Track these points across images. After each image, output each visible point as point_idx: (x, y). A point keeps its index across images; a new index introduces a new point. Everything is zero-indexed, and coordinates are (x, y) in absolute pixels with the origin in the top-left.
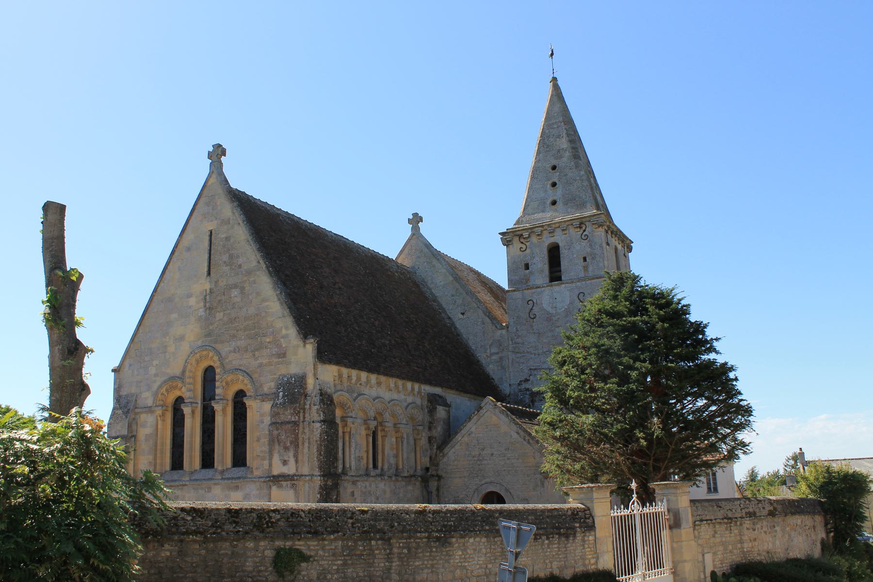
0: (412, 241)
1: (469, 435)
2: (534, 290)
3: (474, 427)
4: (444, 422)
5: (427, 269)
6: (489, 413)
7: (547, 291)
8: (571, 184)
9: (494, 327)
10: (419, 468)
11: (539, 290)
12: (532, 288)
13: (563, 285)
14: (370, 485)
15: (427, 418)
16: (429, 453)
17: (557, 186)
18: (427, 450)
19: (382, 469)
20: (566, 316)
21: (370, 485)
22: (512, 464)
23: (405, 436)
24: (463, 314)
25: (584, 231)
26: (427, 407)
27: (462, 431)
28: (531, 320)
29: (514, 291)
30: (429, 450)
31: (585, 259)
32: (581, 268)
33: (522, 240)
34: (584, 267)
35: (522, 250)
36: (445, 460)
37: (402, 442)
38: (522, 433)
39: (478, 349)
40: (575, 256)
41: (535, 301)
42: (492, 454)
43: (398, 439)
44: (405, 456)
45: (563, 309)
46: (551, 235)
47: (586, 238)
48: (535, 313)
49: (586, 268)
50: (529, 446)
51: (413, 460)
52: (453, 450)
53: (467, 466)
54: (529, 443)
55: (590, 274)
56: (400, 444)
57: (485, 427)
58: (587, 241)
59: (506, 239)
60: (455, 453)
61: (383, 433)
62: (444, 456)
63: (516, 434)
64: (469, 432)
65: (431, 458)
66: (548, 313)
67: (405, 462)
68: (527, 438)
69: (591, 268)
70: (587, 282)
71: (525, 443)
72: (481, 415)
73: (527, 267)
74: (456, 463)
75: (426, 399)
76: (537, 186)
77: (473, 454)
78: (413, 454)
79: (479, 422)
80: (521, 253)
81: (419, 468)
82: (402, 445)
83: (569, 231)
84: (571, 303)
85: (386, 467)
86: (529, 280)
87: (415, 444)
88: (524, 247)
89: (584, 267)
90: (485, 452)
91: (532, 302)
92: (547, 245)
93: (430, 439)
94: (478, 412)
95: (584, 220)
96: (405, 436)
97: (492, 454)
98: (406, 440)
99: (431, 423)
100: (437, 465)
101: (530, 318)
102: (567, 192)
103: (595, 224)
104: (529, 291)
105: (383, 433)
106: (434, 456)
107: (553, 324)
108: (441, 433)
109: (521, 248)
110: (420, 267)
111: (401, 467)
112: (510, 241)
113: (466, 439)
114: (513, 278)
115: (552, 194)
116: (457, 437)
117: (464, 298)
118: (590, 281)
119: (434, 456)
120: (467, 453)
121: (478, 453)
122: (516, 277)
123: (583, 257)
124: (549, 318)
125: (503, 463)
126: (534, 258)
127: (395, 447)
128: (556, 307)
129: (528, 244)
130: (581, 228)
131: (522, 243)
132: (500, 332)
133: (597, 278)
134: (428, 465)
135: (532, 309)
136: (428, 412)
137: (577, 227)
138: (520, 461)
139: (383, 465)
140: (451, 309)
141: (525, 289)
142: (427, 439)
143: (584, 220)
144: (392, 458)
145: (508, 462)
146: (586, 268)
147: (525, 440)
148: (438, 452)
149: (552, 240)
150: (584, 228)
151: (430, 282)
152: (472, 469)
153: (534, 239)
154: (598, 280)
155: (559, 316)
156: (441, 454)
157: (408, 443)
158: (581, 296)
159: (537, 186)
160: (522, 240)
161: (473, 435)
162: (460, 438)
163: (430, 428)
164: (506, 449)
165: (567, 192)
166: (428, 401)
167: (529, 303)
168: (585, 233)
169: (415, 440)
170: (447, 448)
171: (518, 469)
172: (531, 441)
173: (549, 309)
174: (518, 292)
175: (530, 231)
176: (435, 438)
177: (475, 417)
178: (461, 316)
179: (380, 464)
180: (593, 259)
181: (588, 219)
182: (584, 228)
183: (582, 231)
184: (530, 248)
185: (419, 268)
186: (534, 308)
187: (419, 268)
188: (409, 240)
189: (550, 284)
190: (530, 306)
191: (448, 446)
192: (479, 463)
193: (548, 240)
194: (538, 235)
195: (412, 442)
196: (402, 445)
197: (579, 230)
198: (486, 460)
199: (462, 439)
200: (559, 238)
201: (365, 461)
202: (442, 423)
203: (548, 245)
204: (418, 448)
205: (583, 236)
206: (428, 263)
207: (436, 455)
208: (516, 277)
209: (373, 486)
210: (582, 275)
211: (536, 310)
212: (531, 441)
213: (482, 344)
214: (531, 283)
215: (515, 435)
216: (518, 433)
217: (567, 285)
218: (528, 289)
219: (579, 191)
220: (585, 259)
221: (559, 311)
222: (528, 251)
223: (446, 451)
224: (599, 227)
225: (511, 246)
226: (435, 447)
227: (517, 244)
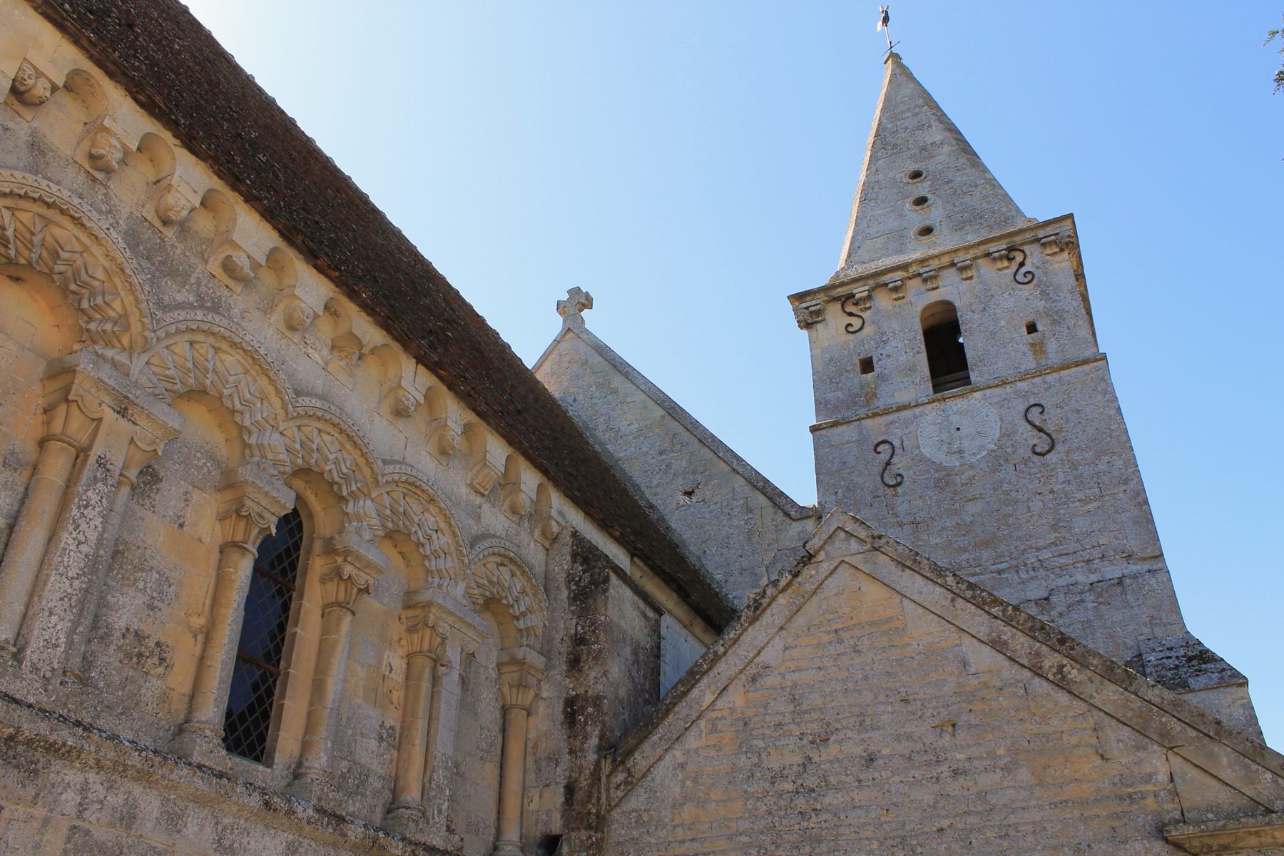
0: (563, 345)
1: (754, 680)
2: (891, 417)
3: (778, 643)
4: (635, 652)
5: (595, 401)
6: (844, 573)
7: (931, 414)
8: (965, 193)
9: (780, 515)
10: (512, 834)
11: (907, 414)
12: (887, 411)
13: (977, 395)
14: (173, 821)
15: (566, 624)
16: (561, 774)
17: (929, 202)
18: (554, 759)
19: (297, 773)
20: (995, 470)
21: (173, 821)
22: (982, 795)
23: (453, 655)
24: (689, 494)
25: (1022, 264)
26: (570, 579)
27: (721, 667)
28: (889, 492)
29: (836, 424)
30: (565, 759)
31: (1032, 328)
32: (1026, 349)
33: (850, 308)
34: (1033, 345)
35: (850, 329)
36: (636, 801)
37: (435, 680)
38: (1021, 643)
39: (732, 579)
40: (1003, 323)
41: (896, 442)
42: (871, 759)
43: (419, 660)
44: (444, 746)
45: (984, 453)
46: (929, 285)
47: (1026, 280)
48: (901, 471)
49: (1038, 349)
50: (1063, 698)
51: (488, 797)
52: (677, 754)
53: (745, 825)
54: (1062, 683)
55: (1054, 358)
56: (426, 685)
57: (826, 638)
58: (1031, 285)
59: (807, 308)
60: (682, 766)
61: (334, 591)
62: (630, 784)
63: (987, 650)
64: (752, 670)
65: (570, 790)
66: (939, 467)
67: (440, 775)
68: (1051, 660)
69: (1052, 346)
70: (1049, 378)
71: (1040, 686)
72: (809, 587)
73: (867, 365)
74: (688, 811)
75: (567, 550)
76: (880, 212)
77: (774, 763)
78: (491, 770)
79: (800, 620)
80: (850, 337)
81: (512, 834)
82: (433, 696)
83: (978, 271)
84: (1006, 435)
85: (319, 760)
86: (875, 395)
87: (504, 730)
88: (856, 323)
89: (1033, 345)
90: (833, 750)
91: (887, 446)
92: (919, 309)
93: (572, 711)
94: (796, 575)
95: (1017, 239)
96: (453, 655)
97: (871, 759)
98: (455, 676)
99: (579, 641)
100: (599, 823)
101: (890, 486)
102: (957, 209)
103: (1050, 243)
104: (879, 420)
105: (331, 587)
106: (584, 783)
107: (955, 493)
108: (622, 692)
109: (850, 325)
110: (580, 397)
111: (413, 794)
112: (818, 313)
113: (737, 698)
114: (829, 396)
115: (917, 218)
116: (695, 693)
117: (692, 454)
118: (1055, 375)
119: (584, 783)
120: (744, 762)
121: (798, 759)
122: (839, 394)
123: (1025, 322)
124: (943, 479)
125: (928, 798)
126: (885, 342)
127: (397, 695)
128: (960, 452)
129: (866, 315)
130: (1010, 260)
131: (851, 314)
132: (796, 527)
133: (1077, 364)
134: (556, 826)
135: (888, 463)
136: (574, 599)
137: (1001, 258)
138: (1024, 775)
139: (305, 746)
140: (657, 486)
141: (868, 417)
142: (559, 707)
143: (1017, 239)
144: (373, 744)
145: (953, 787)
146: (1038, 349)
147: (1037, 671)
148: (606, 767)
149: (934, 297)
150: (1019, 258)
151: (602, 427)
152: (766, 838)
153: (883, 301)
154: (1080, 368)
155: (972, 473)
156: (621, 777)
157: (467, 706)
158: (1034, 415)
159: (880, 212)
160: (850, 308)
161: (772, 680)
162: (709, 698)
163: (575, 663)
164: (939, 728)
165: (957, 209)
166: (574, 556)
167: (880, 449)
168: (1023, 270)
169: (505, 711)
170: (646, 747)
171: (1012, 819)
172: (1073, 673)
173: (940, 457)
174: (844, 427)
175: (871, 282)
176: (597, 701)
177: (782, 600)
178: (683, 499)
179: (286, 741)
180: (1055, 322)
181: (1028, 236)
182: (1019, 258)
183: (1014, 266)
184: (873, 322)
185: (575, 400)
186: (895, 460)
187: (575, 400)
188: (557, 342)
189: (939, 395)
190: (884, 457)
191: (655, 738)
192: (801, 802)
193: (919, 299)
194: (896, 289)
195: (489, 713)
196: (433, 696)
197: (1006, 263)
198: (838, 788)
199: (719, 704)
200: (951, 289)
201: (180, 680)
202: (627, 651)
203: (926, 309)
204: (515, 750)
205: (1020, 277)
206: (599, 386)
207: (596, 776)
208: (839, 394)
209: (191, 829)
210: (1029, 363)
211: (899, 463)
212: (1073, 673)
213: (745, 564)
214: (880, 403)
215: (983, 658)
216: (997, 645)
217: (988, 392)
218: (876, 415)
219: (989, 203)
220: (1032, 328)
221: (970, 459)
222: (868, 330)
223: (640, 760)
224: (1062, 250)
225: (819, 326)
226: (594, 741)
227: (836, 319)
